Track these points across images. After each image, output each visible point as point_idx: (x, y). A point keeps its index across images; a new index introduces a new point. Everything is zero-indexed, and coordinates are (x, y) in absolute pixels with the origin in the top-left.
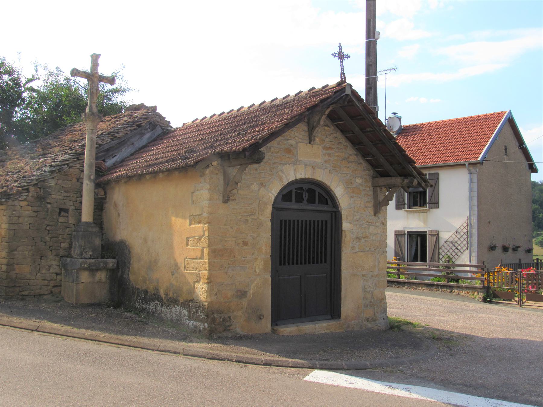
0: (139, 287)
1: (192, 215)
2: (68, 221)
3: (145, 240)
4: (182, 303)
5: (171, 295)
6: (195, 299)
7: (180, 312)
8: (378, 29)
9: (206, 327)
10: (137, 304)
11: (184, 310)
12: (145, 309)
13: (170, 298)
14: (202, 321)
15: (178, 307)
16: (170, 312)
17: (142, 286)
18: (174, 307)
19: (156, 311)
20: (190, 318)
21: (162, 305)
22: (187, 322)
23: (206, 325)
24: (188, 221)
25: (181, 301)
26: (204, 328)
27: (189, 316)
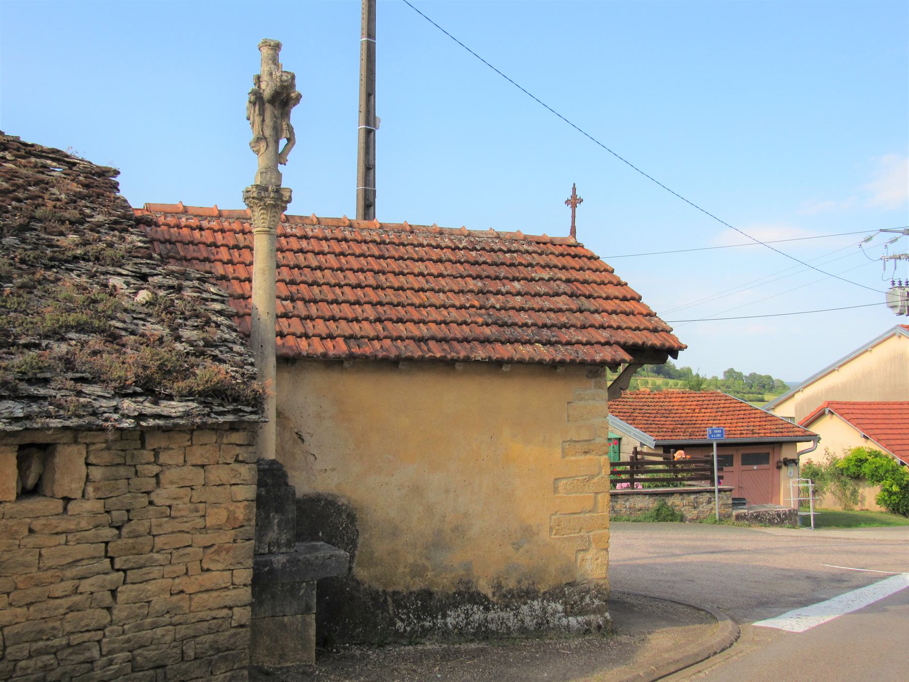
0: (399, 588)
1: (571, 441)
2: (56, 657)
3: (417, 491)
4: (545, 593)
5: (511, 584)
6: (578, 580)
7: (544, 610)
8: (378, 114)
9: (609, 618)
10: (399, 624)
11: (553, 604)
12: (431, 629)
13: (510, 591)
14: (598, 611)
15: (535, 603)
16: (516, 615)
17: (404, 583)
18: (525, 604)
19: (468, 624)
20: (567, 614)
21: (487, 609)
22: (564, 621)
23: (607, 614)
24: (559, 451)
25: (542, 591)
26: (606, 621)
27: (565, 611)
